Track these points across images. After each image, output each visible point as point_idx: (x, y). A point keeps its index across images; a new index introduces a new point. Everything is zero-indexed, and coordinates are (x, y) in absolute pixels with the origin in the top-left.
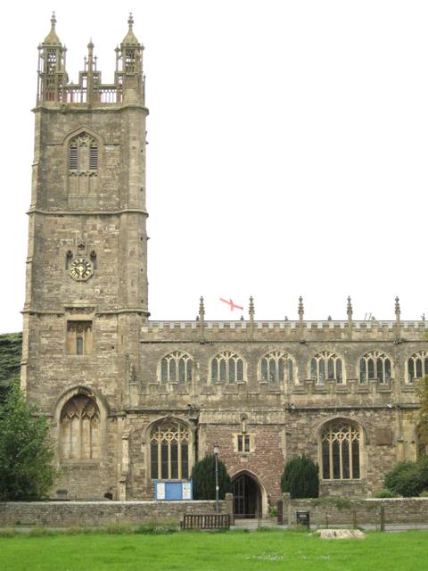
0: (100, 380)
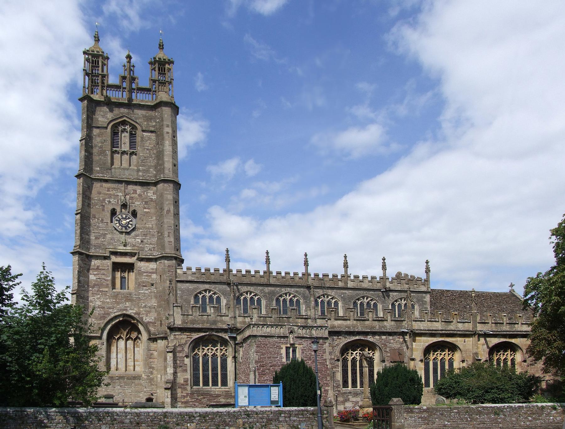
0: (142, 309)
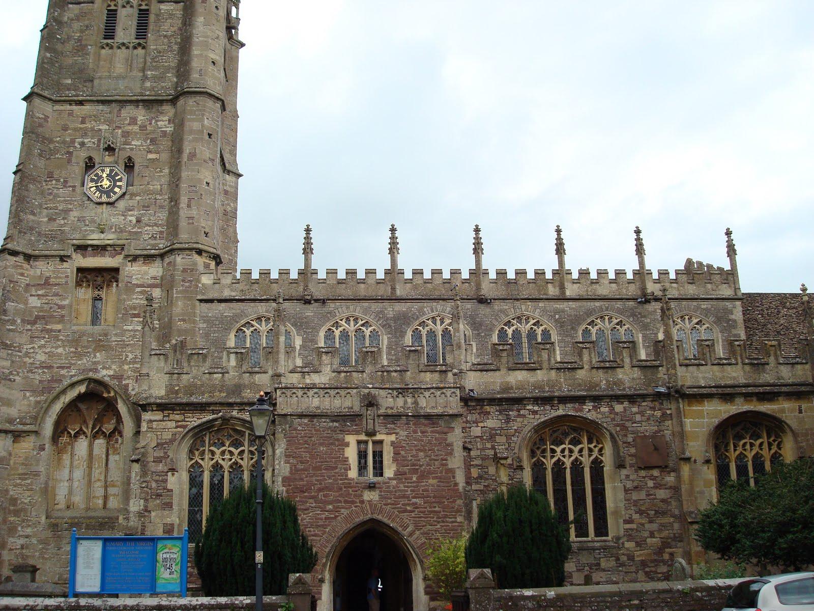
0: (126, 367)
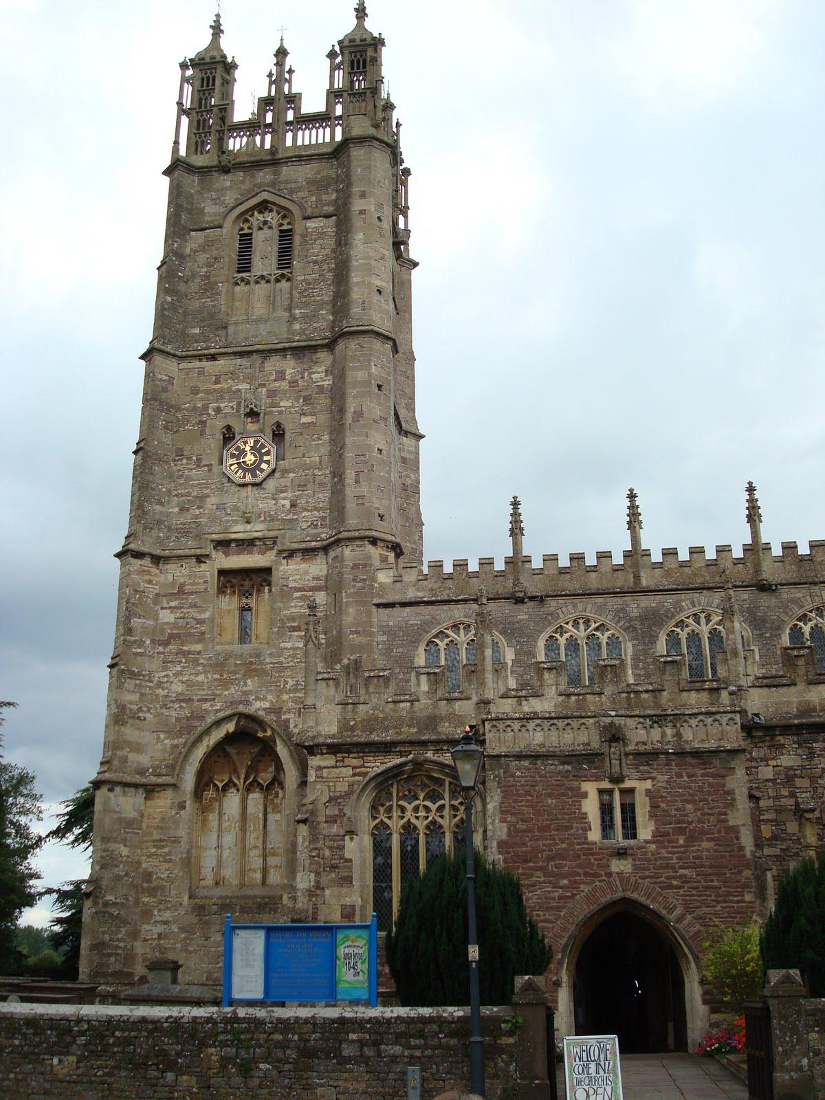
0: (285, 697)
